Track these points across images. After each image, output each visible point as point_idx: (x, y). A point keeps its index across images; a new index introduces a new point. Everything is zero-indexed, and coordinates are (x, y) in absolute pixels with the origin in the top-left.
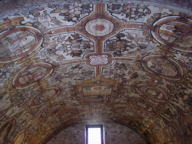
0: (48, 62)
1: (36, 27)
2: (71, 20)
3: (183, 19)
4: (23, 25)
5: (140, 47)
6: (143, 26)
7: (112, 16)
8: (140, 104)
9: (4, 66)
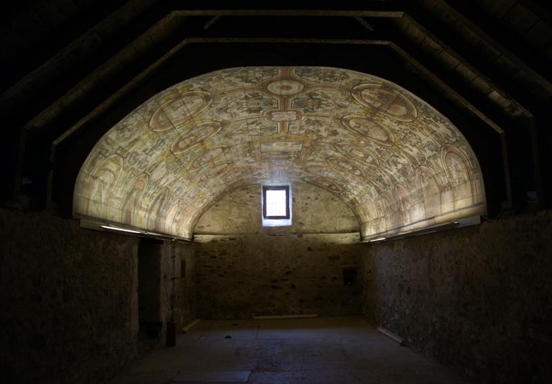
0: (216, 121)
1: (206, 91)
2: (250, 82)
5: (339, 106)
8: (344, 164)
9: (164, 134)
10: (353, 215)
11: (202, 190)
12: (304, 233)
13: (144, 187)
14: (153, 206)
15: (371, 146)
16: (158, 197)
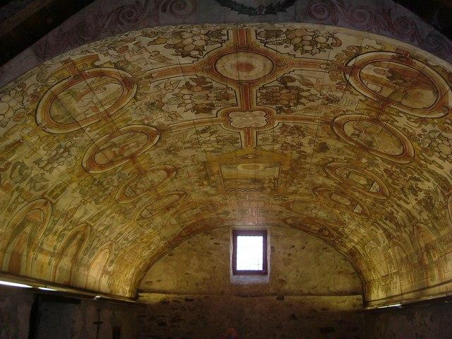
1: (122, 69)
3: (404, 59)
4: (97, 67)
6: (328, 66)
7: (266, 48)
8: (338, 197)
9: (65, 138)
10: (352, 270)
11: (147, 232)
12: (287, 293)
13: (45, 220)
14: (64, 249)
15: (377, 165)
16: (74, 237)
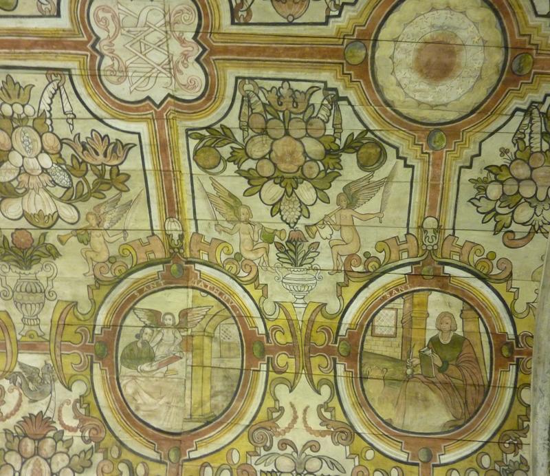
7: (509, 110)
